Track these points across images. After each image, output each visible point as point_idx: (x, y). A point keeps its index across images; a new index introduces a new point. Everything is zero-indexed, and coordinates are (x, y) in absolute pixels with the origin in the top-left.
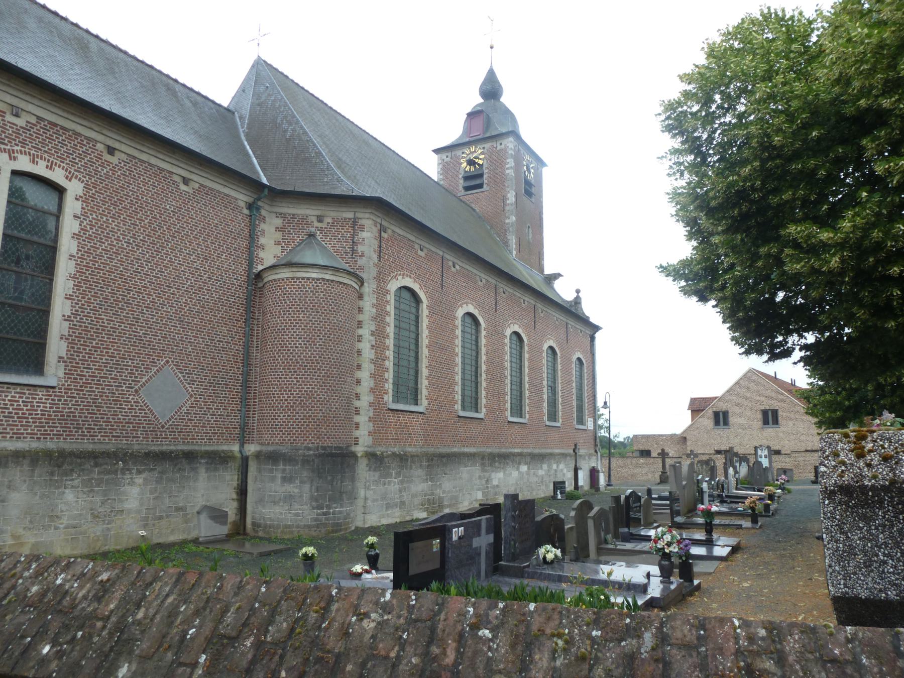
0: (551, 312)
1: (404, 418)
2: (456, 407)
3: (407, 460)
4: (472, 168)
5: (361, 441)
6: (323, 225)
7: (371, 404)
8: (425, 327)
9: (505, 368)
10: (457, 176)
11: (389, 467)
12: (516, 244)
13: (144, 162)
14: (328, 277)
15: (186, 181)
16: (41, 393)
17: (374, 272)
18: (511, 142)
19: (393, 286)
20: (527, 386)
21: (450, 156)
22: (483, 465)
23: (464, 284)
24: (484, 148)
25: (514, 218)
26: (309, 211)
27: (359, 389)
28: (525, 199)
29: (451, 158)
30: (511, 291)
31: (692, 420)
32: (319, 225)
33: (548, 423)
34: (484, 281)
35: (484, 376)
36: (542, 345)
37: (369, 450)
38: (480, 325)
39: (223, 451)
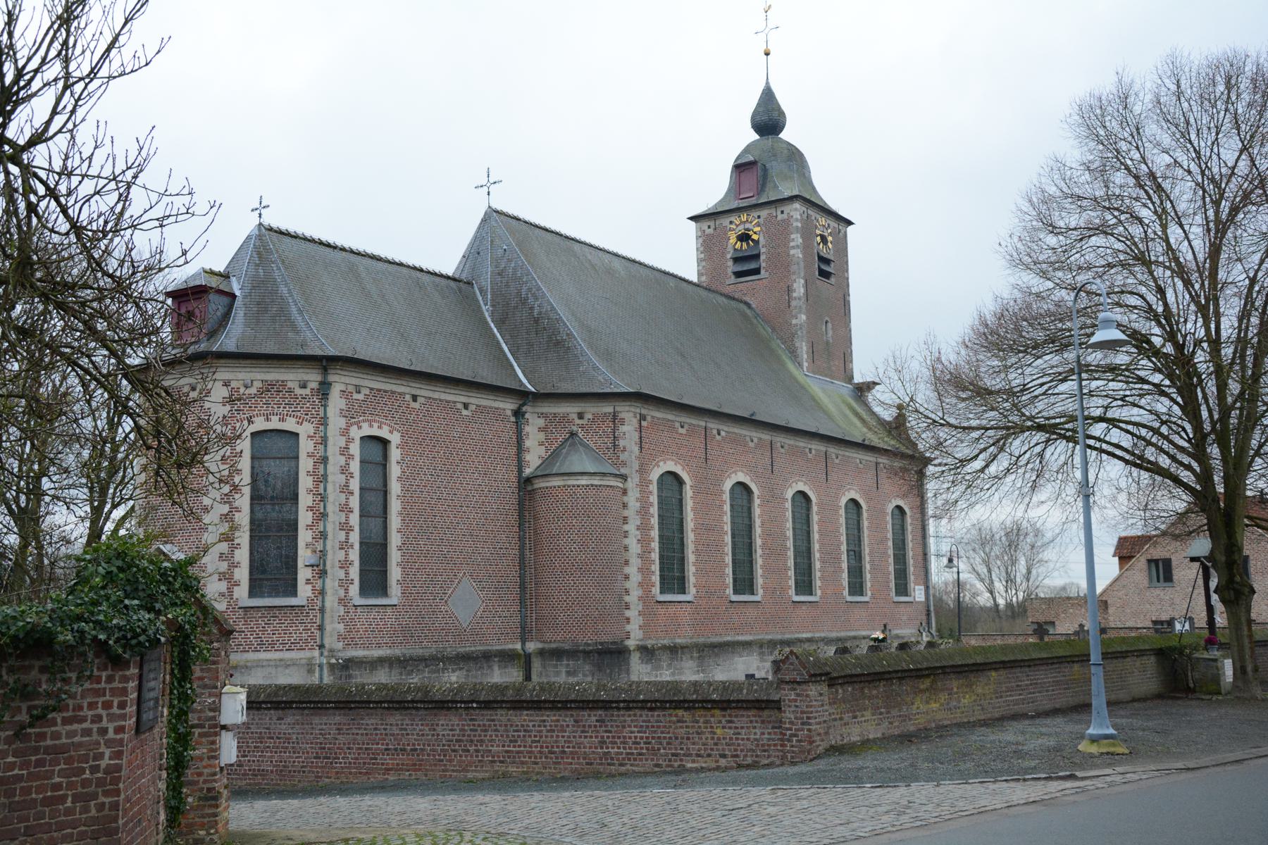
0: (851, 455)
1: (672, 609)
2: (727, 591)
3: (677, 652)
4: (745, 245)
5: (632, 636)
6: (584, 422)
7: (640, 598)
8: (689, 509)
9: (787, 538)
10: (723, 255)
11: (660, 660)
12: (807, 353)
13: (436, 399)
14: (596, 482)
15: (466, 406)
16: (389, 610)
17: (636, 466)
18: (796, 209)
19: (655, 475)
20: (817, 555)
21: (713, 227)
22: (762, 654)
23: (731, 451)
24: (759, 217)
25: (804, 317)
26: (570, 409)
27: (628, 585)
28: (821, 283)
29: (715, 229)
30: (792, 442)
31: (1121, 568)
32: (580, 422)
33: (849, 599)
34: (756, 440)
35: (759, 552)
36: (838, 498)
37: (640, 643)
38: (752, 492)
39: (510, 650)
